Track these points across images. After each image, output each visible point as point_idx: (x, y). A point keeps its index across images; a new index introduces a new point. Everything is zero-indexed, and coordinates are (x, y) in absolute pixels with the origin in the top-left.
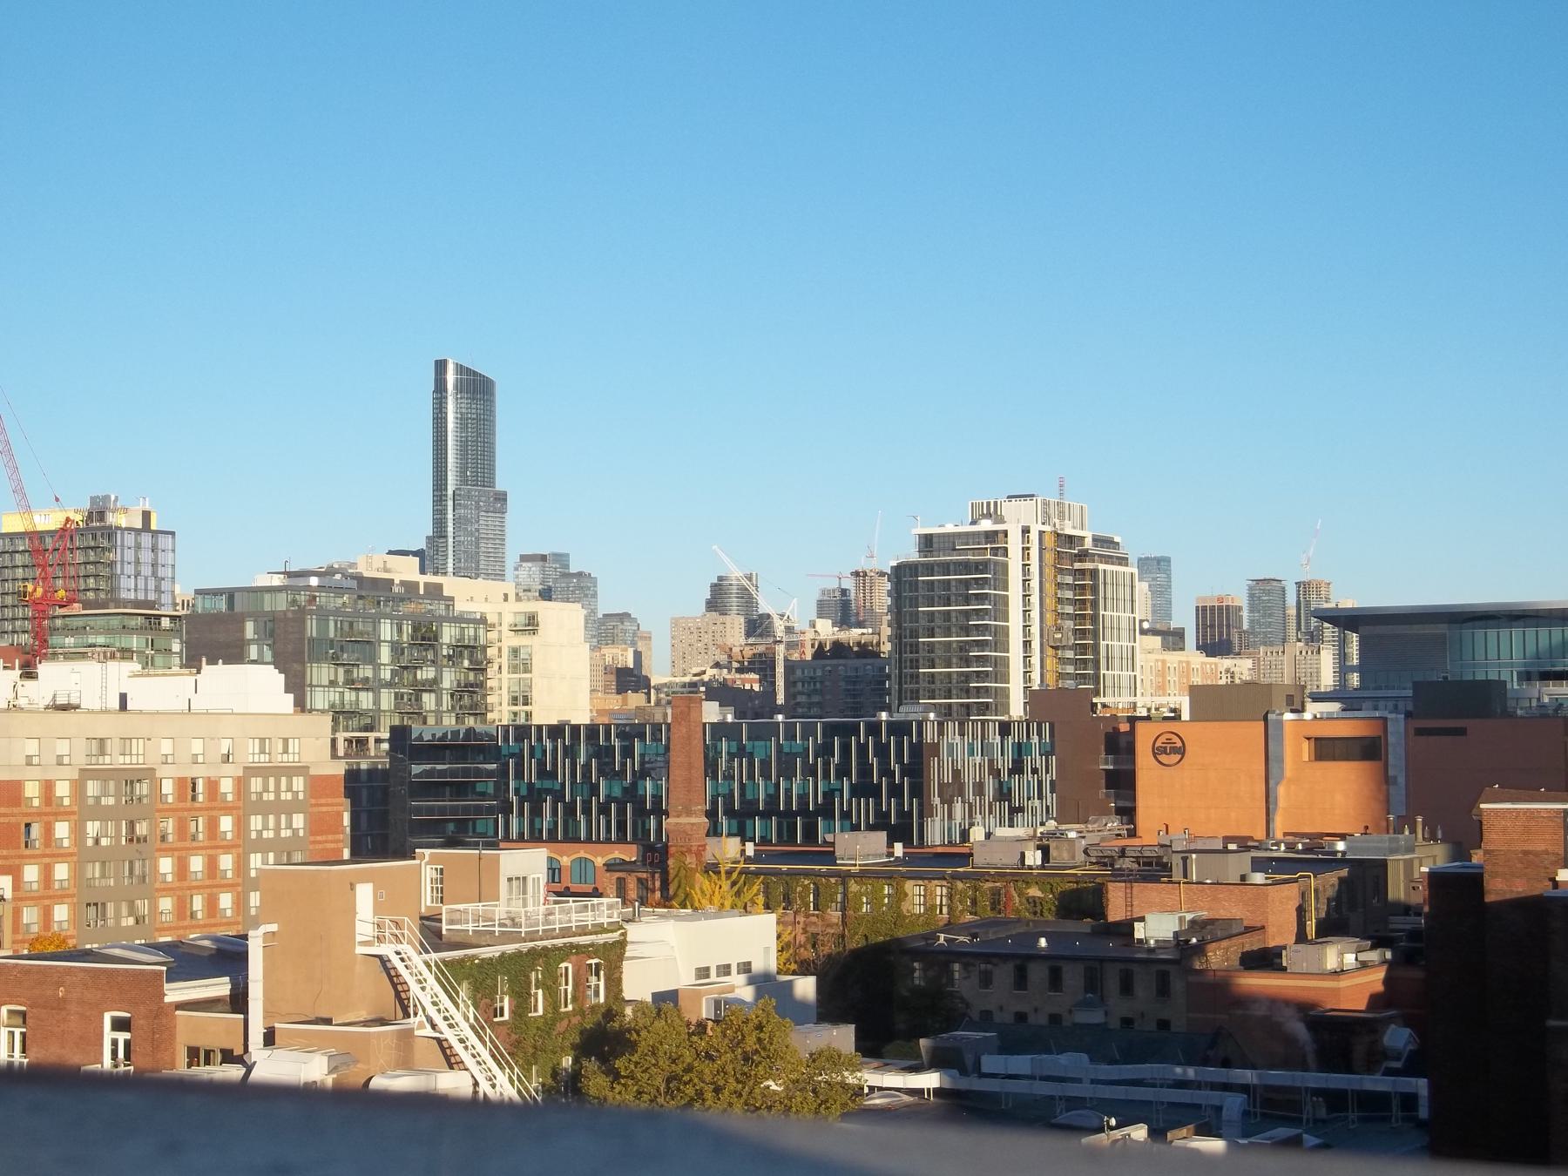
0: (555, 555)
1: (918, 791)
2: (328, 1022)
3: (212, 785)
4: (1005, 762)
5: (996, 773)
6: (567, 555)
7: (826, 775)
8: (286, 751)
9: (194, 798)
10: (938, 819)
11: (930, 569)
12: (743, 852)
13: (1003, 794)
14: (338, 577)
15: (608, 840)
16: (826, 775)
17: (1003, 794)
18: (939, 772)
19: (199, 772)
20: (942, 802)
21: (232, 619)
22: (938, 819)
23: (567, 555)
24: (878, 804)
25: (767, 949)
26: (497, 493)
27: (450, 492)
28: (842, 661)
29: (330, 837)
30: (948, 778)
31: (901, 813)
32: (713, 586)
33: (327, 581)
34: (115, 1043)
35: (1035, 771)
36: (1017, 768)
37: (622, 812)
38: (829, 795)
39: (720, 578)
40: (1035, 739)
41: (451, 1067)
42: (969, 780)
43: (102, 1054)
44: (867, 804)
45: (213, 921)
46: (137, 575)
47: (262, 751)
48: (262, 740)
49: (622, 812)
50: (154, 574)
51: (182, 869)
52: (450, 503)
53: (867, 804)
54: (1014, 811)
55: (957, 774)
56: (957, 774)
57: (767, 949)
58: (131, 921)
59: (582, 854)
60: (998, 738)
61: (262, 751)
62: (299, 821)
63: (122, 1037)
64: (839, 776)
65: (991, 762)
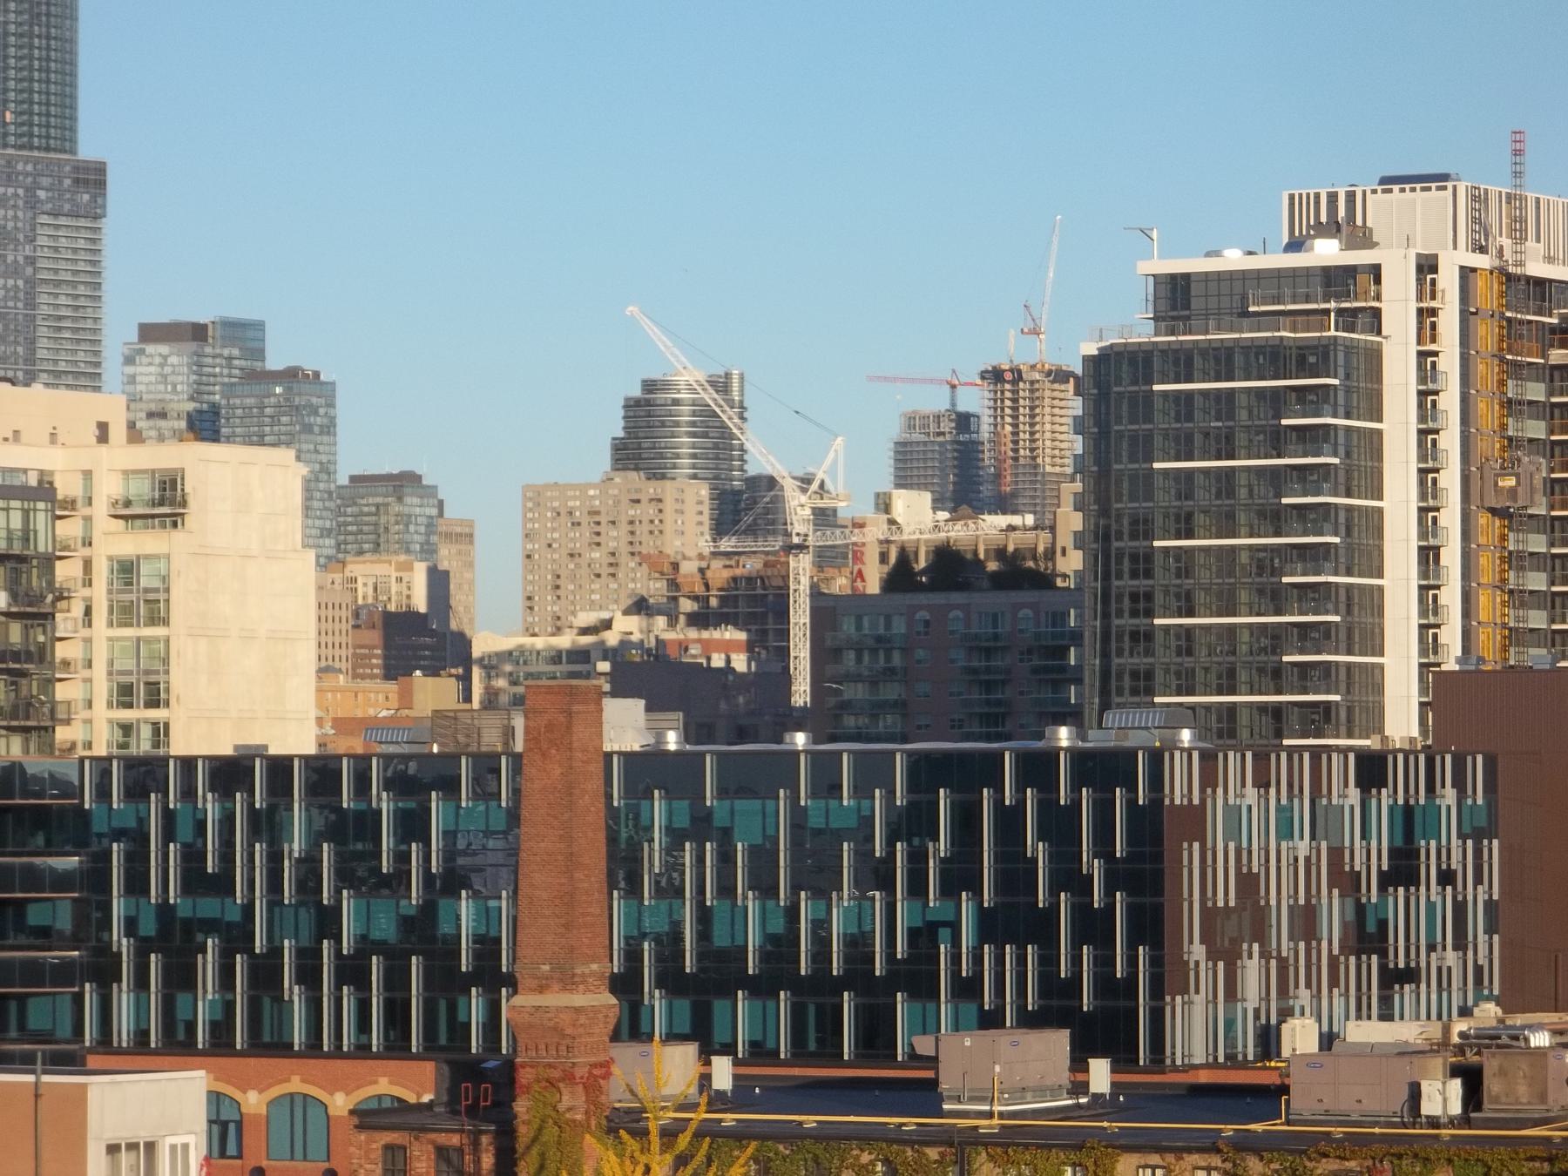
1: (1152, 926)
4: (1370, 854)
5: (1347, 882)
7: (917, 887)
11: (1182, 363)
13: (1367, 936)
16: (917, 887)
17: (1367, 936)
18: (1203, 880)
20: (1212, 956)
24: (1048, 961)
28: (957, 598)
30: (1226, 895)
31: (1105, 983)
35: (1446, 878)
36: (1403, 870)
37: (396, 980)
38: (924, 936)
40: (1449, 796)
42: (1280, 899)
44: (1021, 960)
49: (396, 980)
53: (1021, 960)
54: (1396, 978)
55: (1248, 884)
56: (1248, 884)
59: (295, 1085)
60: (1354, 794)
64: (950, 890)
65: (1336, 854)
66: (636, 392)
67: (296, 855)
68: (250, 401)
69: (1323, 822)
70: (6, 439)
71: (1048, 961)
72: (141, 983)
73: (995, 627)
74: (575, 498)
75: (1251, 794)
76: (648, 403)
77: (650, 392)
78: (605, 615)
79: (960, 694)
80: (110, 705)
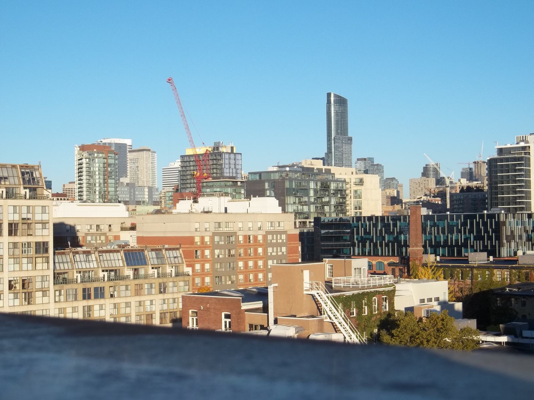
0: (369, 158)
2: (295, 316)
3: (255, 237)
5: (526, 231)
7: (465, 233)
8: (279, 226)
9: (249, 242)
10: (505, 248)
11: (501, 160)
12: (436, 259)
14: (296, 167)
15: (389, 256)
16: (465, 233)
18: (506, 231)
19: (251, 233)
21: (261, 182)
22: (505, 248)
24: (484, 243)
25: (445, 293)
26: (348, 138)
27: (333, 138)
28: (470, 193)
29: (295, 255)
30: (509, 233)
32: (424, 168)
33: (292, 169)
34: (226, 322)
37: (393, 246)
38: (466, 239)
39: (427, 165)
41: (336, 332)
42: (517, 234)
43: (222, 326)
44: (480, 243)
45: (256, 282)
46: (230, 168)
47: (272, 226)
48: (271, 222)
49: (393, 246)
50: (235, 168)
51: (246, 265)
52: (333, 141)
53: (480, 243)
55: (512, 232)
56: (512, 232)
57: (445, 293)
58: (230, 282)
59: (380, 260)
61: (272, 226)
62: (284, 249)
63: (228, 320)
64: (469, 233)
69: (523, 223)
71: (484, 243)
72: (359, 247)
75: (512, 219)
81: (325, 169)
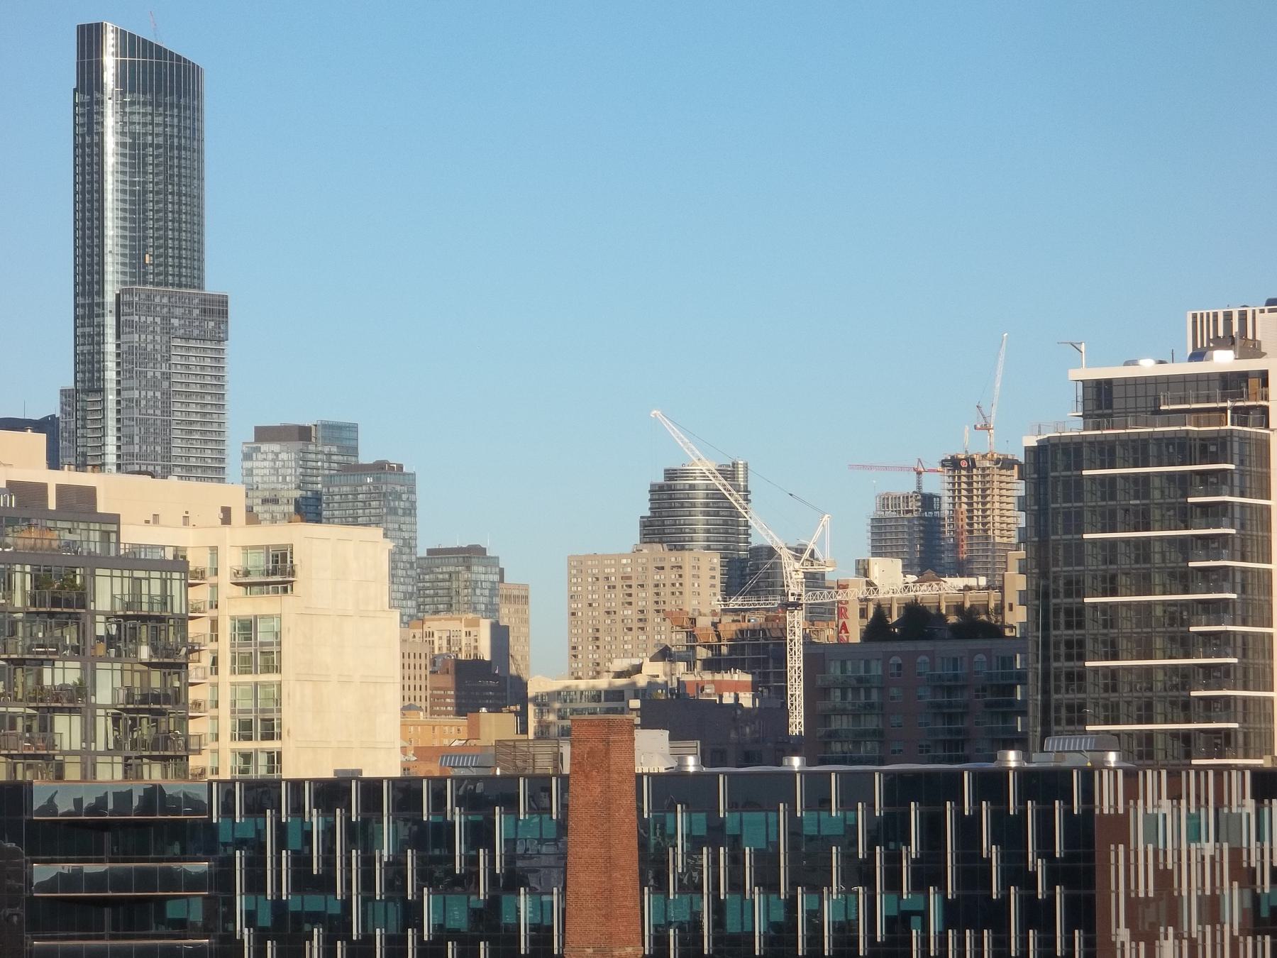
6: (353, 428)
23: (353, 428)
27: (110, 298)
32: (656, 490)
39: (671, 474)
52: (110, 321)
66: (660, 479)
67: (386, 859)
68: (345, 489)
70: (147, 522)
73: (955, 668)
74: (610, 566)
76: (670, 488)
77: (671, 479)
78: (636, 661)
79: (926, 724)
80: (233, 738)
81: (61, 489)
